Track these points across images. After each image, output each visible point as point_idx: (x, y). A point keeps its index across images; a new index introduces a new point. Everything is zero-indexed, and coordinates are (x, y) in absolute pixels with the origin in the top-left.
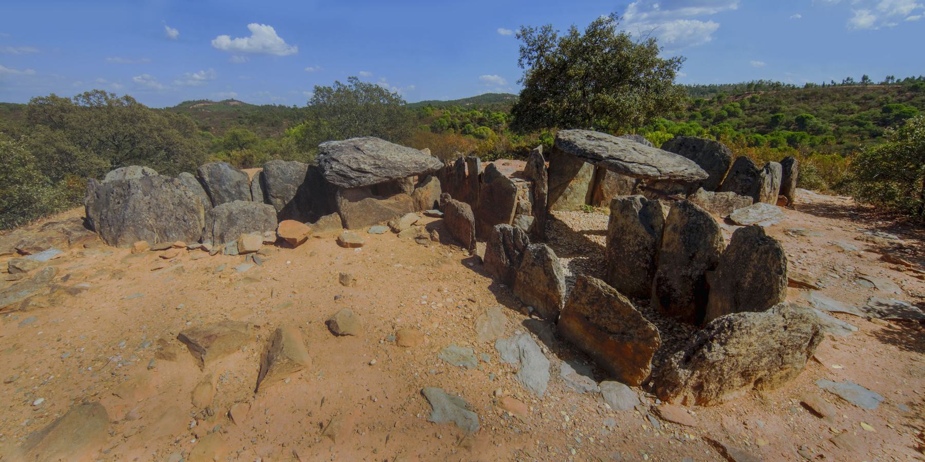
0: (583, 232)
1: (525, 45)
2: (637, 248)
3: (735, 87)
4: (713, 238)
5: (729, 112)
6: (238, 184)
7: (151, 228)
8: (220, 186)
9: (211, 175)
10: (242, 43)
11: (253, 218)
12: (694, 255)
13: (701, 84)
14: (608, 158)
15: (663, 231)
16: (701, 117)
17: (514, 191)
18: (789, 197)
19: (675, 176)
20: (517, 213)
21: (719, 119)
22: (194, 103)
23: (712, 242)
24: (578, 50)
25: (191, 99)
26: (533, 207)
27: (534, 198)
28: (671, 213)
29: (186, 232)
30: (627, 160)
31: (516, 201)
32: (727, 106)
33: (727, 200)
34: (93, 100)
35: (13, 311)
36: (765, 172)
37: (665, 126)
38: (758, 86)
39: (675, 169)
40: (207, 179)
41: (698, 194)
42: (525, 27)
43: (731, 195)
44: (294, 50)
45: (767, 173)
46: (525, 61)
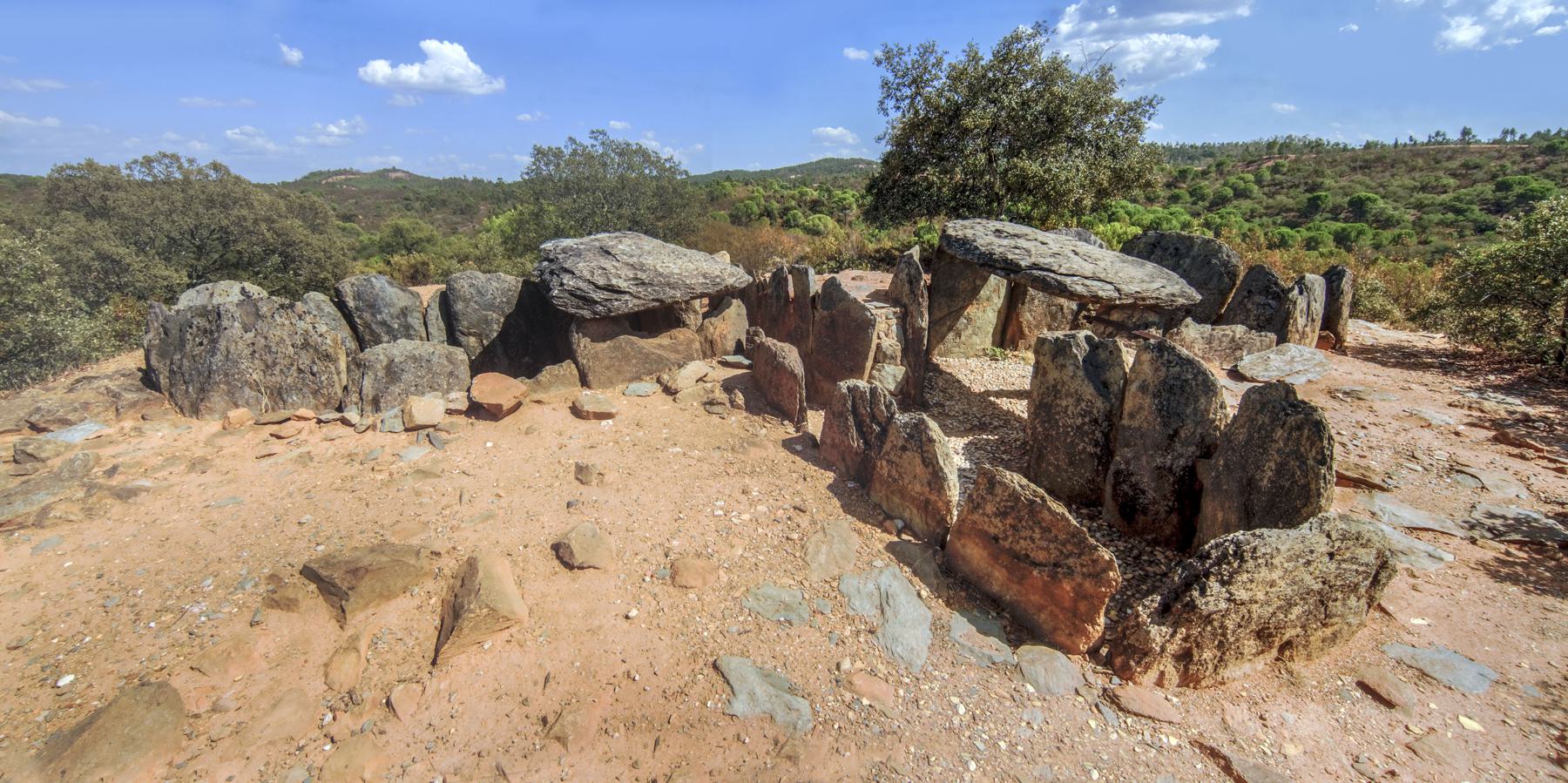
0: (988, 393)
1: (891, 77)
2: (1079, 421)
3: (1246, 147)
4: (1209, 403)
5: (1235, 190)
6: (404, 312)
7: (255, 386)
8: (373, 315)
9: (358, 296)
10: (411, 73)
11: (430, 370)
12: (1176, 432)
13: (1189, 142)
14: (1030, 268)
15: (1123, 392)
16: (1187, 198)
17: (871, 324)
18: (1337, 334)
19: (1143, 299)
20: (876, 361)
21: (1219, 202)
22: (329, 174)
23: (1208, 411)
24: (980, 86)
25: (325, 169)
26: (904, 351)
27: (905, 331)
28: (1137, 361)
29: (315, 393)
30: (1062, 270)
31: (875, 341)
32: (1232, 179)
33: (1233, 340)
34: (158, 169)
35: (22, 526)
36: (1296, 291)
37: (1128, 213)
38: (1286, 146)
39: (1145, 286)
40: (351, 304)
41: (1183, 329)
42: (891, 45)
43: (1239, 330)
44: (499, 84)
45: (1301, 293)
46: (891, 103)
